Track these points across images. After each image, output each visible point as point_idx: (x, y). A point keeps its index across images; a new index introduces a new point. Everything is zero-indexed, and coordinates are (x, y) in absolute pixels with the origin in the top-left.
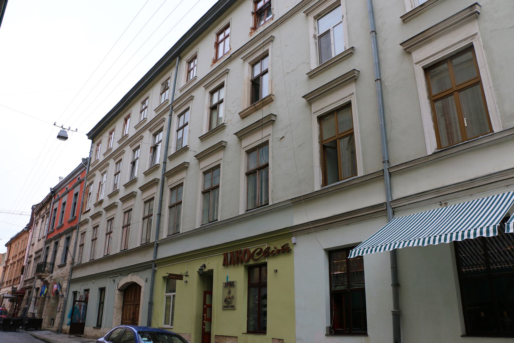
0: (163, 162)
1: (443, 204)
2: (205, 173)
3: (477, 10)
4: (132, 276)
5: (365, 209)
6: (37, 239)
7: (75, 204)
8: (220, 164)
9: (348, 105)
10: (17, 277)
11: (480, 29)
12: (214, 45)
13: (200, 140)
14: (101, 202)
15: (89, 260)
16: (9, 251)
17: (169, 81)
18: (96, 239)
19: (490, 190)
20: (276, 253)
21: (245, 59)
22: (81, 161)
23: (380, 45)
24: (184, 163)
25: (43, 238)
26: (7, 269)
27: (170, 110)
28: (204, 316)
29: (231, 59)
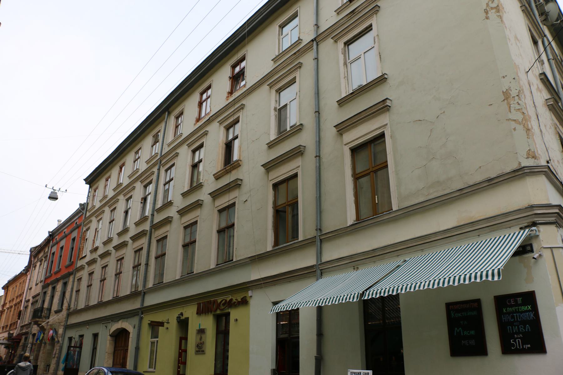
0: (151, 215)
1: (356, 268)
2: (185, 228)
3: (388, 104)
4: (122, 322)
5: (300, 270)
6: (34, 284)
7: (73, 248)
8: (197, 221)
9: (295, 176)
10: (14, 322)
11: (390, 120)
12: (197, 105)
13: (182, 196)
14: (96, 249)
15: (84, 305)
16: (6, 294)
17: (159, 134)
18: (91, 285)
19: (387, 258)
20: (236, 305)
21: (271, 86)
22: (78, 207)
23: (321, 124)
24: (168, 217)
25: (41, 282)
26: (4, 314)
27: (158, 164)
28: (179, 360)
29: (209, 121)
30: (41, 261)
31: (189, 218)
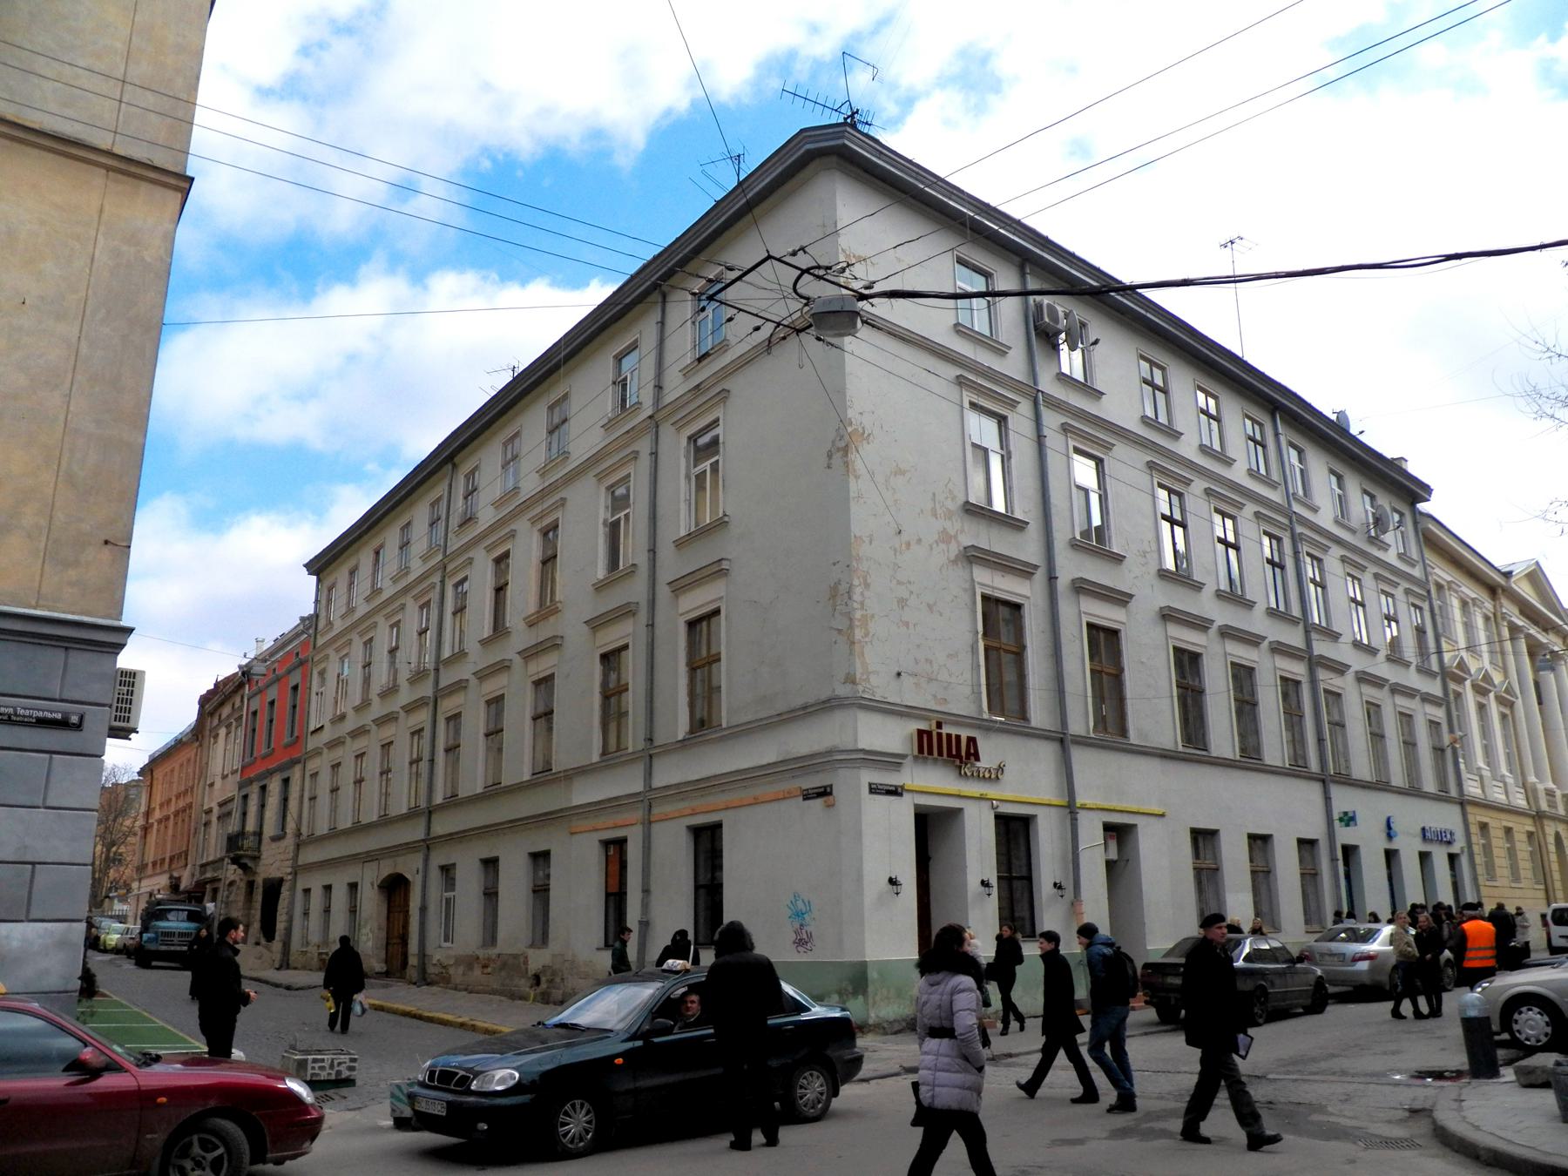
14: (342, 717)
18: (338, 789)
30: (228, 726)
31: (541, 667)
